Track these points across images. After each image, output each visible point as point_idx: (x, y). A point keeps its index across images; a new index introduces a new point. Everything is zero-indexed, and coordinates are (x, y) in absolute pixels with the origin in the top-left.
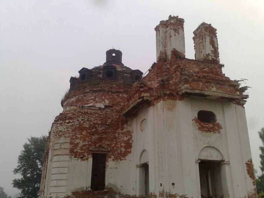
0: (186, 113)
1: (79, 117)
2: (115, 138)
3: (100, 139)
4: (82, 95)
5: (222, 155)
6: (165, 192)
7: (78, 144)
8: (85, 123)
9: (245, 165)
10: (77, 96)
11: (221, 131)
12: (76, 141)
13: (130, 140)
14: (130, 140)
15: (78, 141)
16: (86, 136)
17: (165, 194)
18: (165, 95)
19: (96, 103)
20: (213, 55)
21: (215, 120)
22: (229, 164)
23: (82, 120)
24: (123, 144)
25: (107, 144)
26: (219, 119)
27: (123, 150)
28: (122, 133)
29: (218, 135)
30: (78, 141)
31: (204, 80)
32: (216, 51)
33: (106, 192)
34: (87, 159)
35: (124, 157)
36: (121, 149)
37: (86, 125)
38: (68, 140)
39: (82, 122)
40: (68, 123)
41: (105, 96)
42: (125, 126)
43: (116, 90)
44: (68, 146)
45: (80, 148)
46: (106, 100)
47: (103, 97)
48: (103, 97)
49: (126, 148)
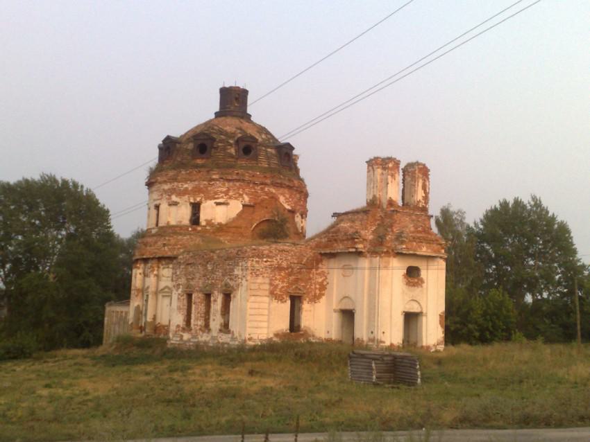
0: (397, 268)
1: (277, 255)
2: (310, 279)
3: (297, 280)
4: (205, 182)
5: (421, 308)
7: (277, 285)
9: (438, 316)
10: (196, 183)
11: (424, 285)
15: (277, 282)
16: (284, 277)
18: (383, 252)
19: (230, 198)
20: (423, 201)
21: (419, 275)
22: (426, 316)
23: (281, 259)
24: (318, 286)
26: (423, 274)
27: (318, 292)
28: (317, 274)
29: (420, 289)
30: (277, 282)
31: (418, 240)
33: (302, 335)
34: (286, 301)
37: (284, 264)
38: (267, 281)
40: (266, 262)
41: (244, 189)
42: (320, 265)
43: (260, 180)
44: (267, 287)
46: (244, 196)
47: (241, 190)
48: (241, 190)
49: (320, 290)
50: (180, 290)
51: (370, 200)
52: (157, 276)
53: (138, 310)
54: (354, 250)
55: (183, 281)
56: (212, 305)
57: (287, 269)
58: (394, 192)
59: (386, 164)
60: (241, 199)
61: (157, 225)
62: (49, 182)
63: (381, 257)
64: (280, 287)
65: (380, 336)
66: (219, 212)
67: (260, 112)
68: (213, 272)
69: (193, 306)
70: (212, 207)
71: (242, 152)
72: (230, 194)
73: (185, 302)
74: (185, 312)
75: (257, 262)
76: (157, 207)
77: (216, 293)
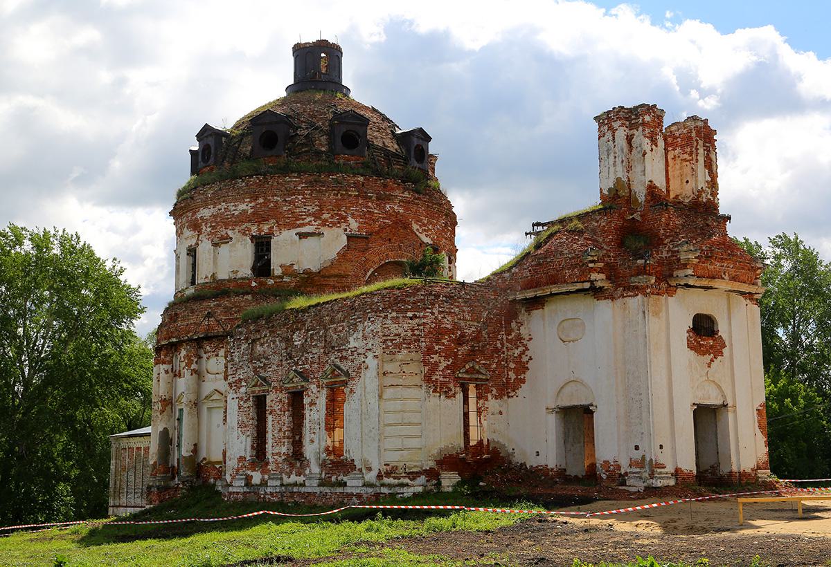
6: (648, 459)
8: (445, 320)
9: (756, 412)
11: (725, 351)
12: (433, 358)
13: (523, 356)
14: (523, 356)
15: (436, 358)
17: (647, 462)
23: (440, 312)
24: (512, 365)
25: (483, 364)
27: (512, 375)
32: (713, 184)
34: (454, 395)
35: (514, 391)
36: (508, 375)
39: (440, 318)
40: (411, 318)
45: (441, 373)
50: (243, 390)
51: (610, 190)
52: (196, 372)
53: (166, 440)
54: (587, 285)
55: (246, 372)
56: (307, 412)
57: (453, 331)
58: (652, 170)
59: (637, 117)
60: (344, 226)
61: (193, 283)
62: (28, 246)
63: (645, 295)
64: (442, 366)
65: (654, 454)
66: (304, 249)
67: (361, 83)
68: (304, 349)
69: (270, 418)
70: (293, 243)
71: (339, 143)
72: (326, 216)
73: (252, 412)
74: (251, 431)
75: (395, 320)
76: (192, 252)
77: (313, 387)
